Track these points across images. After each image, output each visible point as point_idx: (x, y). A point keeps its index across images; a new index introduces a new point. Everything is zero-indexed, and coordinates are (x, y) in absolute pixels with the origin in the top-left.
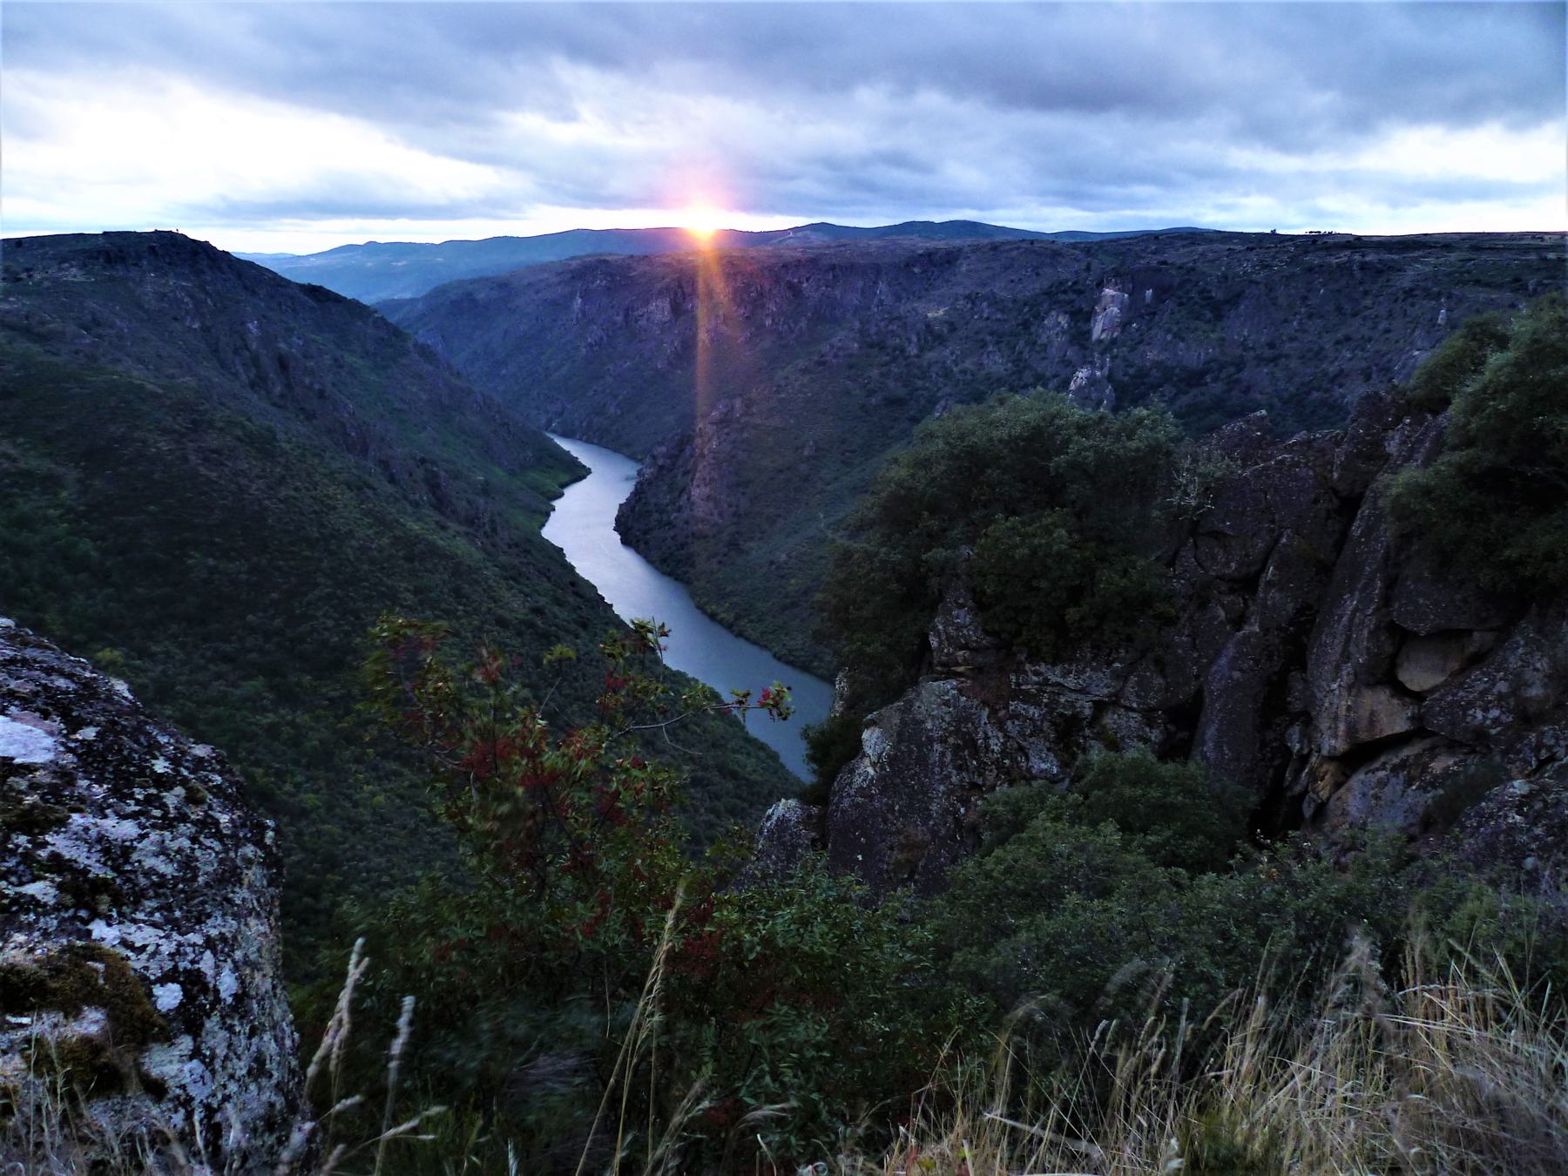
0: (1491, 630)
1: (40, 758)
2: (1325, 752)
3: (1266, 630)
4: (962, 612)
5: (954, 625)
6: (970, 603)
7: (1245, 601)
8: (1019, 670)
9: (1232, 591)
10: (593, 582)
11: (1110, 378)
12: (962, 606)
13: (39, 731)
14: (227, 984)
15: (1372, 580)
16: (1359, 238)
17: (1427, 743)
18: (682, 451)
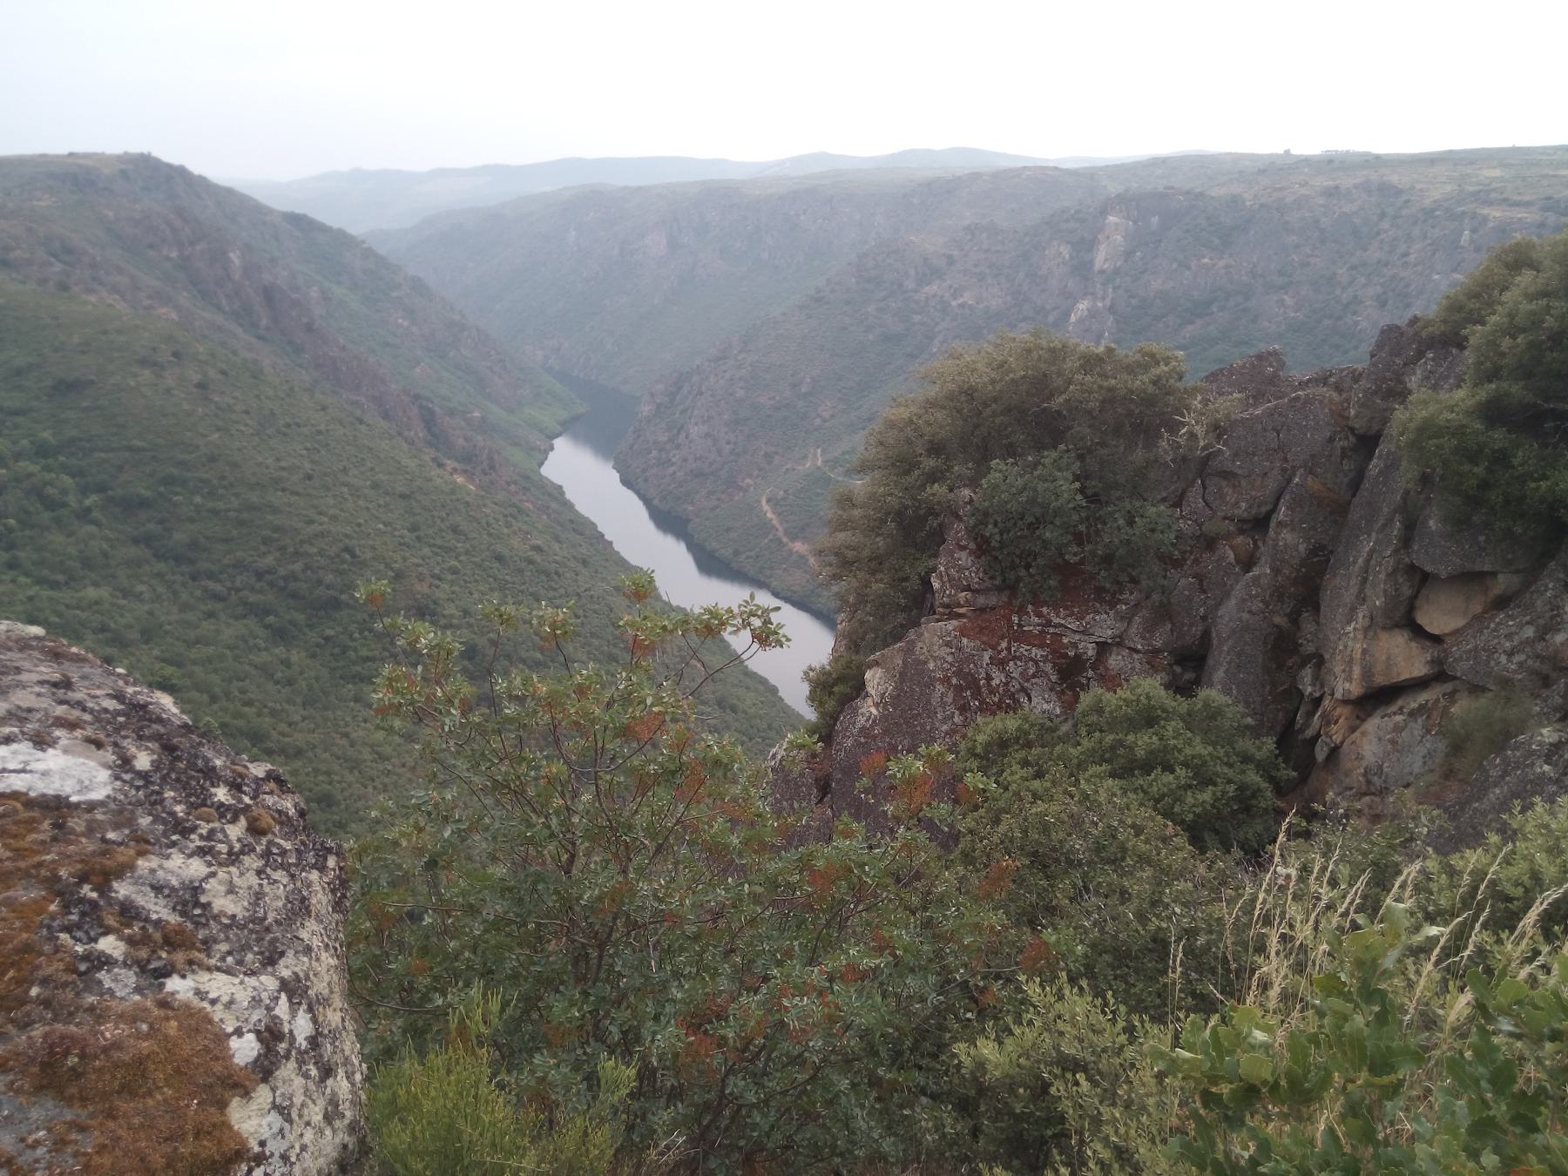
0: (1517, 572)
1: (98, 795)
2: (1338, 695)
3: (1276, 571)
4: (964, 555)
5: (954, 569)
6: (972, 546)
7: (1255, 542)
8: (1021, 611)
9: (1241, 531)
10: (593, 519)
11: (1112, 309)
12: (963, 548)
13: (92, 764)
14: (302, 1027)
15: (1390, 520)
16: (1378, 157)
17: (1448, 687)
18: (680, 388)
